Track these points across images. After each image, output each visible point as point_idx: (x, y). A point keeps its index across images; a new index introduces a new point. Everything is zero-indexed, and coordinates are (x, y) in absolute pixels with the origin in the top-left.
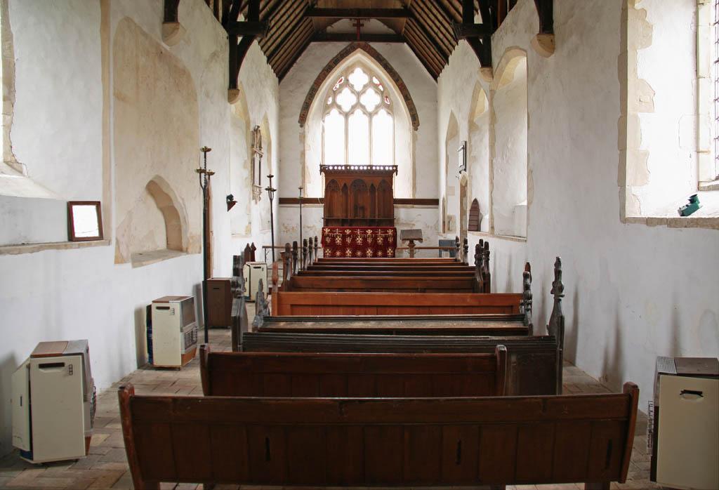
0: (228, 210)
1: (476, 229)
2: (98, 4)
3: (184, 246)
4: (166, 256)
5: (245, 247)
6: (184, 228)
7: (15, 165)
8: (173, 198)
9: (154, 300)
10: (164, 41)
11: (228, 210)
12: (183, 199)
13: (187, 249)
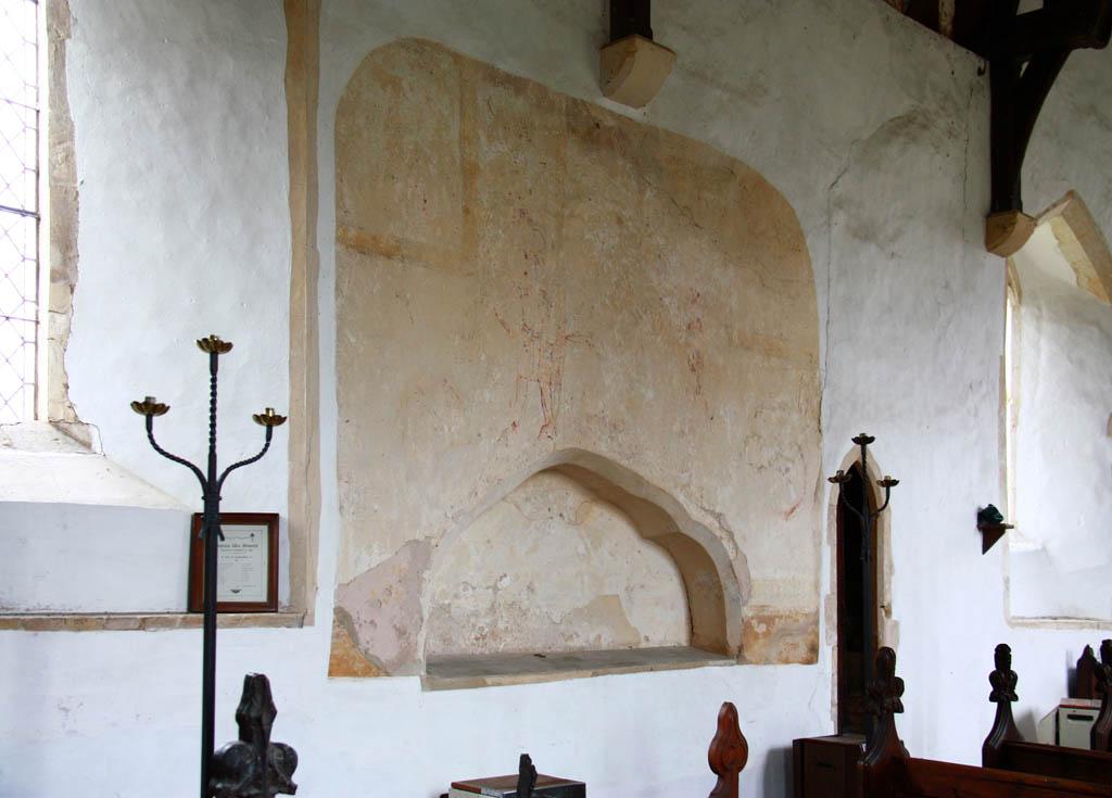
0: (985, 551)
1: (136, 626)
2: (279, 15)
3: (733, 642)
4: (640, 664)
5: (1079, 654)
6: (729, 591)
7: (75, 429)
8: (670, 510)
9: (456, 780)
10: (607, 94)
11: (985, 551)
12: (719, 517)
13: (741, 649)
